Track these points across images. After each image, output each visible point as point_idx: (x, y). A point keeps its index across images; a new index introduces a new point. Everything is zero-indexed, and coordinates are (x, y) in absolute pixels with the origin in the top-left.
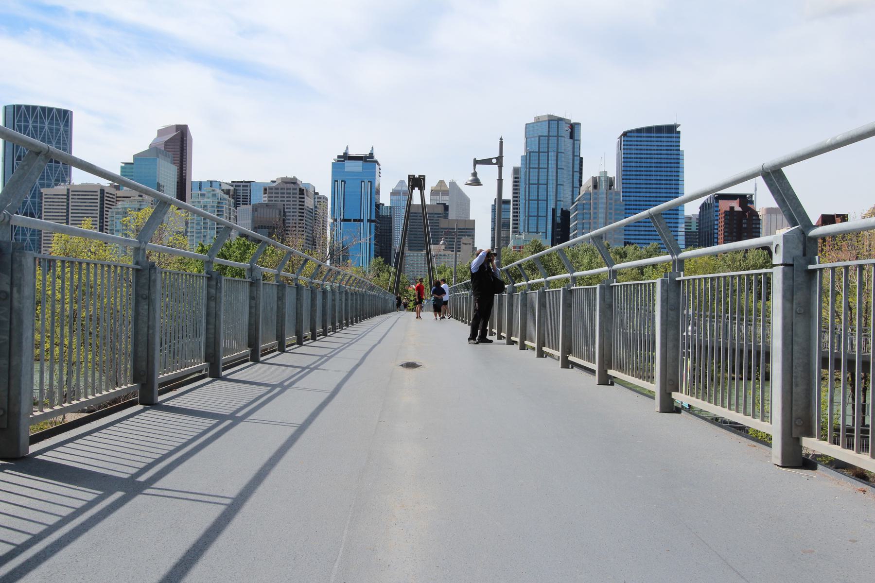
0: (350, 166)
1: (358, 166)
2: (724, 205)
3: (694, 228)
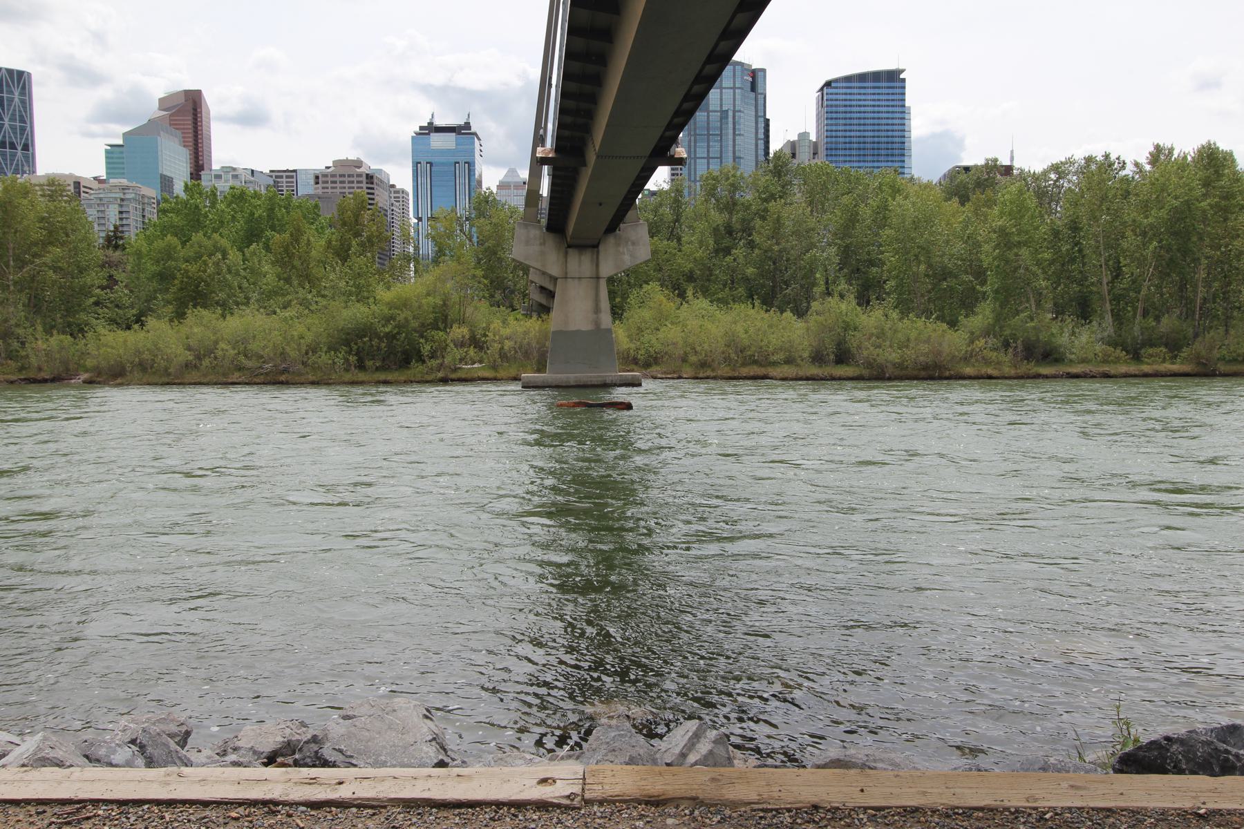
1: (448, 141)
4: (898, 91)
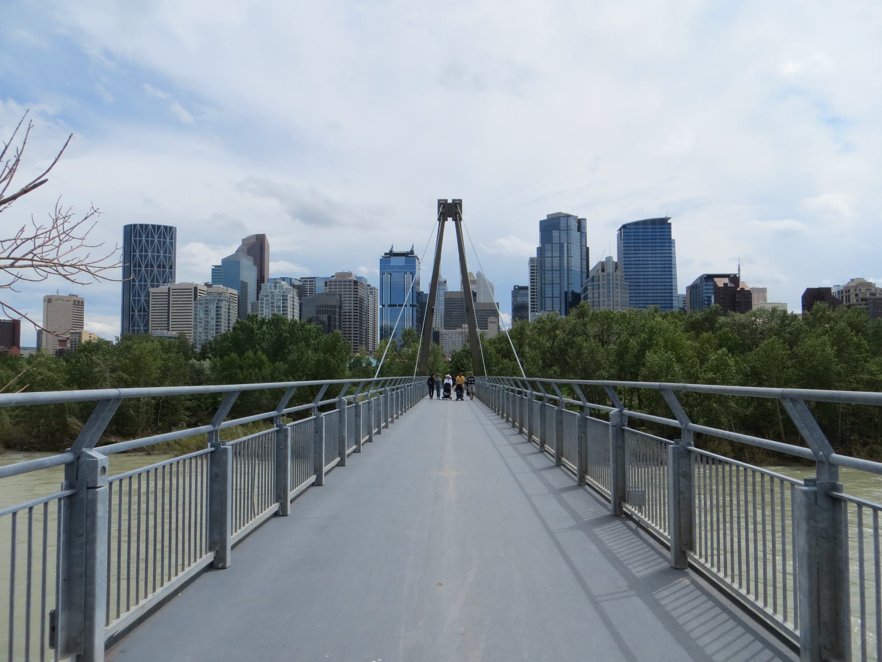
0: (394, 261)
1: (401, 261)
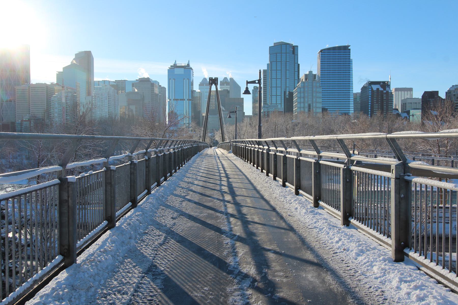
0: (177, 71)
1: (181, 71)
2: (375, 87)
3: (358, 100)
4: (347, 56)
